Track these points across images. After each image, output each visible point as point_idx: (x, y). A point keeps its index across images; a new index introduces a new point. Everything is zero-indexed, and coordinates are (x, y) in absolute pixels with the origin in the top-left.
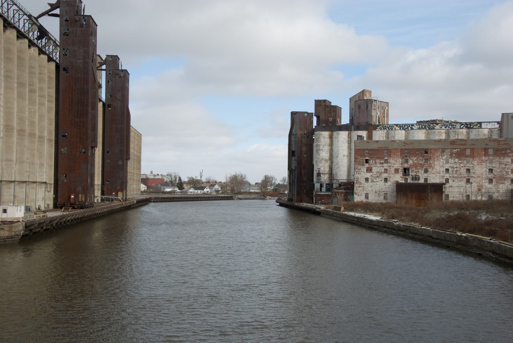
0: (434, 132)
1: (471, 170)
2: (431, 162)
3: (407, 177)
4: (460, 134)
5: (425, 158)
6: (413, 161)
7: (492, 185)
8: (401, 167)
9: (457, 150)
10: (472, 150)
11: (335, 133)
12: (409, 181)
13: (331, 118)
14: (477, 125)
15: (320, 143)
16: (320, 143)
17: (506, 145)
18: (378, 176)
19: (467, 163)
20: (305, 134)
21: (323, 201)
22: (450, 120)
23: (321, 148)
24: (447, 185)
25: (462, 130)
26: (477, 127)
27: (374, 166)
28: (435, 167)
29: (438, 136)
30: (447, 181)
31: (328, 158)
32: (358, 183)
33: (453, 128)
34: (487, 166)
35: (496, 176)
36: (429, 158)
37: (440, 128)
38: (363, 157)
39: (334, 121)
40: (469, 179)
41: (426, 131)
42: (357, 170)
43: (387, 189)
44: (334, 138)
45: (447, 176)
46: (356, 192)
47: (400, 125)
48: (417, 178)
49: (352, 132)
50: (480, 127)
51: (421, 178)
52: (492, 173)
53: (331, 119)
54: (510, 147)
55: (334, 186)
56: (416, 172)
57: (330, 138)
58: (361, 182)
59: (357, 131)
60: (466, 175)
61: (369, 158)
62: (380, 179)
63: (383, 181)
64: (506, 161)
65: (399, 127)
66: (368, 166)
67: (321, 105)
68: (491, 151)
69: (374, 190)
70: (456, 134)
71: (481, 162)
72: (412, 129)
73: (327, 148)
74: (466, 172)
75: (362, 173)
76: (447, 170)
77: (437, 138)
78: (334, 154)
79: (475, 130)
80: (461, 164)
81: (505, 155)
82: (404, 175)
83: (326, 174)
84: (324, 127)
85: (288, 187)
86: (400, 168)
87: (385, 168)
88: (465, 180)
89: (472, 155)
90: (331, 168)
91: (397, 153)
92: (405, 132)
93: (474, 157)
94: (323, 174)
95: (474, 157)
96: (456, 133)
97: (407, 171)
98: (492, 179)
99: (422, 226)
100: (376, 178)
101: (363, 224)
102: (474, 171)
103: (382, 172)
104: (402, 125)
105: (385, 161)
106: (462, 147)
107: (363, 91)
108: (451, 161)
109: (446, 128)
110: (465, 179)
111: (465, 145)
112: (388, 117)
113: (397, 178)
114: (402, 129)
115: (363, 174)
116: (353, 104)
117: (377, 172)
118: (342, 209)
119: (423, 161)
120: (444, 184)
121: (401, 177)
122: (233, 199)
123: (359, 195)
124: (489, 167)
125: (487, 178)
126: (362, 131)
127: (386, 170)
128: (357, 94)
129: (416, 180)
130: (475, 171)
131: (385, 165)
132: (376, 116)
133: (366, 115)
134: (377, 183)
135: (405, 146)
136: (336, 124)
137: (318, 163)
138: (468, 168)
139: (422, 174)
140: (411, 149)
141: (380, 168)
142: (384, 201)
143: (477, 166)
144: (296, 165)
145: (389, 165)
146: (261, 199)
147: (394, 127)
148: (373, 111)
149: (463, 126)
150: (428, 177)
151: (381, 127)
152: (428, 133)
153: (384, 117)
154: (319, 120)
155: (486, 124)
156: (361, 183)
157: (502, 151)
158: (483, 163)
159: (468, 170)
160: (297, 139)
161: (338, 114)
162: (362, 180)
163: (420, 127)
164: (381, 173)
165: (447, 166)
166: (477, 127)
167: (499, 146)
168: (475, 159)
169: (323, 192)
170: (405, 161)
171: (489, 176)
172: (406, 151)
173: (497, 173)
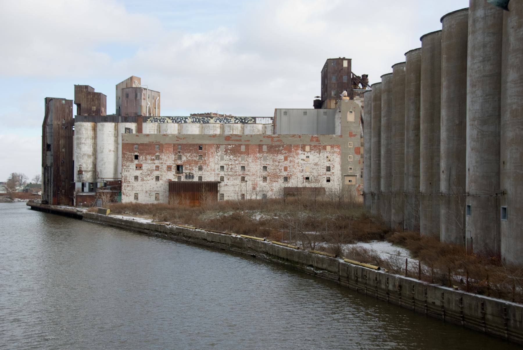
0: (209, 127)
2: (205, 159)
3: (181, 175)
4: (235, 129)
5: (199, 154)
6: (187, 158)
7: (267, 183)
8: (174, 164)
9: (232, 146)
10: (247, 146)
11: (99, 125)
12: (183, 179)
14: (251, 120)
17: (279, 141)
18: (148, 174)
19: (242, 160)
20: (63, 125)
21: (85, 203)
23: (83, 141)
26: (252, 122)
27: (144, 163)
28: (210, 164)
30: (222, 179)
32: (127, 182)
33: (228, 122)
37: (215, 122)
38: (132, 153)
40: (244, 177)
41: (200, 124)
42: (125, 167)
43: (159, 189)
44: (98, 130)
45: (222, 174)
46: (124, 192)
47: (173, 118)
50: (255, 122)
51: (195, 176)
52: (266, 170)
53: (94, 108)
54: (282, 144)
55: (99, 185)
56: (190, 169)
58: (129, 180)
59: (125, 123)
60: (241, 173)
61: (138, 154)
62: (151, 178)
63: (155, 179)
64: (279, 158)
66: (137, 163)
67: (82, 91)
68: (265, 148)
69: (144, 190)
70: (231, 129)
71: (255, 159)
72: (185, 122)
73: (90, 142)
75: (131, 171)
76: (222, 167)
78: (98, 148)
80: (236, 162)
81: (278, 152)
83: (89, 171)
84: (86, 117)
86: (173, 165)
87: (156, 165)
90: (95, 165)
91: (170, 149)
92: (179, 125)
93: (249, 154)
94: (85, 171)
96: (231, 128)
97: (180, 169)
98: (266, 177)
99: (196, 229)
100: (146, 176)
102: (249, 169)
103: (153, 170)
104: (175, 118)
105: (156, 157)
106: (237, 143)
107: (131, 78)
108: (226, 157)
109: (220, 122)
110: (240, 177)
112: (159, 108)
117: (148, 170)
118: (108, 211)
119: (198, 158)
120: (219, 182)
121: (173, 175)
123: (127, 196)
124: (263, 164)
125: (262, 176)
127: (157, 167)
128: (124, 81)
129: (189, 178)
131: (156, 162)
134: (148, 182)
135: (178, 140)
136: (100, 115)
137: (79, 159)
138: (243, 165)
139: (196, 172)
140: (184, 144)
141: (152, 165)
142: (156, 202)
145: (161, 161)
147: (165, 119)
148: (143, 100)
149: (238, 120)
151: (152, 119)
152: (202, 127)
153: (155, 108)
154: (80, 108)
155: (260, 119)
156: (129, 182)
158: (258, 161)
159: (243, 168)
161: (103, 103)
163: (193, 121)
164: (152, 171)
165: (222, 163)
166: (252, 122)
168: (249, 156)
170: (178, 157)
172: (179, 147)
173: (271, 171)
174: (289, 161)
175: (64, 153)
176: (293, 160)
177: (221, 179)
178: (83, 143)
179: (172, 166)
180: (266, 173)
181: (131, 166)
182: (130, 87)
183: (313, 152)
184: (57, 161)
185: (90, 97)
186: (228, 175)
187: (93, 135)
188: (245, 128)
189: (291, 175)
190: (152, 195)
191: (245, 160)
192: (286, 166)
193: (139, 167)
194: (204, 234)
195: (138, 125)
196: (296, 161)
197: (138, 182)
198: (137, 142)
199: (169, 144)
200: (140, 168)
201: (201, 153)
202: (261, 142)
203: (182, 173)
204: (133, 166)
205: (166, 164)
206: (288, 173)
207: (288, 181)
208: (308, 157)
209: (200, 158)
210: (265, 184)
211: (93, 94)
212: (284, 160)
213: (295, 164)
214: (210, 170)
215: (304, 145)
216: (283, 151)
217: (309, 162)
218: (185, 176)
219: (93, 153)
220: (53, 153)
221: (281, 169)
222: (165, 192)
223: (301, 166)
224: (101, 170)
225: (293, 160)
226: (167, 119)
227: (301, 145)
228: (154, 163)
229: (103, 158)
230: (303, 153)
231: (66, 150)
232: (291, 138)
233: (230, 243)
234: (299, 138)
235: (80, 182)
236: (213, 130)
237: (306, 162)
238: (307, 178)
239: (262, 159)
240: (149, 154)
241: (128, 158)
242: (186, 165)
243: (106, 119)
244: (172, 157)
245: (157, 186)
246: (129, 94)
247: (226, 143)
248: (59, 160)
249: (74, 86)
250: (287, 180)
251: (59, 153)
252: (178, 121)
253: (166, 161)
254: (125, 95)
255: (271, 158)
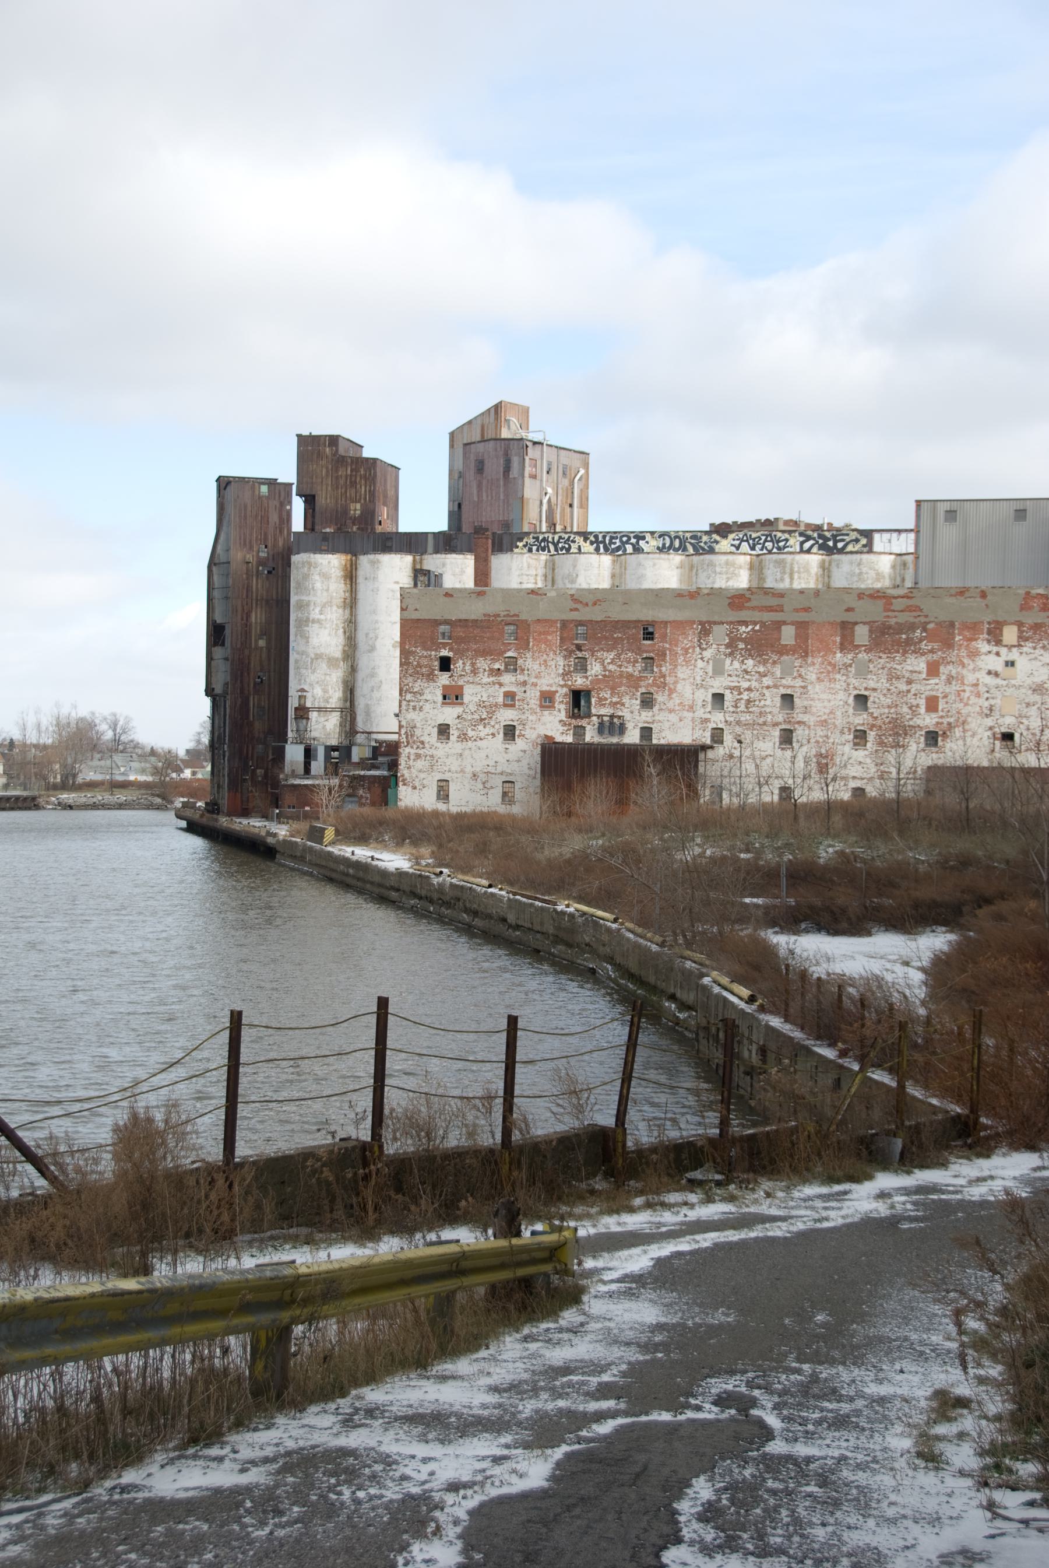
0: (711, 564)
1: (795, 700)
2: (664, 669)
3: (583, 722)
4: (799, 572)
5: (645, 655)
6: (604, 667)
7: (866, 752)
8: (562, 686)
9: (750, 627)
10: (801, 626)
11: (364, 560)
12: (591, 736)
13: (358, 506)
14: (857, 541)
15: (311, 598)
16: (311, 598)
17: (910, 611)
18: (482, 720)
19: (785, 674)
20: (261, 562)
21: (307, 808)
22: (826, 521)
23: (315, 614)
24: (720, 751)
25: (806, 556)
26: (858, 547)
27: (468, 682)
28: (679, 687)
29: (724, 576)
30: (718, 736)
31: (338, 654)
32: (414, 742)
33: (779, 548)
34: (848, 684)
35: (879, 722)
36: (657, 655)
37: (733, 549)
38: (431, 650)
39: (368, 517)
40: (791, 731)
41: (683, 557)
42: (409, 697)
43: (514, 767)
44: (360, 580)
45: (718, 719)
46: (407, 775)
47: (596, 537)
48: (614, 725)
49: (425, 557)
50: (869, 548)
51: (629, 726)
52: (866, 709)
53: (356, 509)
54: (923, 619)
55: (356, 755)
56: (614, 705)
57: (345, 577)
58: (422, 739)
59: (443, 556)
60: (780, 718)
61: (451, 654)
62: (489, 730)
63: (502, 735)
64: (910, 668)
65: (592, 543)
66: (447, 683)
67: (320, 455)
68: (862, 634)
69: (469, 769)
70: (784, 573)
71: (829, 672)
72: (637, 550)
73: (335, 616)
74: (782, 707)
75: (427, 707)
76: (719, 698)
77: (720, 583)
78: (361, 637)
79: (849, 556)
80: (764, 679)
81: (908, 647)
82: (573, 716)
83: (333, 710)
84: (325, 537)
85: (209, 756)
86: (559, 689)
87: (507, 689)
88: (776, 733)
89: (800, 647)
90: (350, 691)
91: (549, 638)
92: (614, 561)
93: (807, 655)
94: (320, 710)
95: (805, 654)
96: (784, 567)
97: (583, 703)
98: (865, 732)
99: (490, 886)
100: (474, 725)
101: (368, 886)
102: (806, 703)
103: (496, 705)
104: (604, 537)
105: (506, 665)
106: (768, 617)
107: (497, 408)
108: (733, 665)
109: (753, 548)
110: (778, 729)
111: (780, 609)
112: (584, 505)
113: (548, 726)
114: (602, 550)
115: (431, 711)
116: (459, 450)
117: (481, 705)
118: (330, 833)
119: (639, 666)
120: (704, 748)
121: (561, 721)
122: (37, 807)
123: (415, 788)
124: (855, 688)
125: (850, 730)
126: (461, 556)
127: (510, 696)
128: (476, 418)
129: (611, 733)
130: (811, 703)
131: (507, 678)
132: (538, 503)
133: (502, 497)
134: (479, 743)
135: (576, 609)
136: (373, 529)
137: (303, 671)
138: (789, 692)
139: (632, 712)
140: (597, 622)
141: (491, 690)
142: (502, 809)
143: (817, 686)
144: (229, 679)
145: (521, 678)
146: (150, 807)
147: (574, 542)
148: (527, 480)
149: (811, 542)
150: (653, 723)
151: (531, 541)
152: (692, 567)
153: (571, 506)
154: (314, 510)
155: (886, 536)
156: (422, 743)
157: (898, 634)
158: (838, 676)
159: (788, 700)
160: (231, 581)
161: (385, 491)
162: (426, 732)
163: (664, 545)
164: (492, 709)
165: (718, 685)
166: (858, 547)
167: (888, 617)
168: (810, 660)
169: (315, 777)
170: (576, 664)
171: (857, 721)
172: (581, 630)
173: (883, 711)
174: (943, 677)
175: (264, 655)
176: (958, 673)
177: (713, 736)
178: (313, 621)
179: (557, 692)
180: (865, 716)
181: (427, 691)
182: (494, 437)
183: (1028, 647)
184: (242, 675)
185: (345, 472)
186: (738, 723)
187: (347, 594)
188: (834, 569)
189: (949, 724)
190: (492, 788)
191: (795, 674)
192: (934, 693)
193: (452, 696)
194: (501, 901)
195: (477, 560)
196: (970, 678)
197: (450, 744)
198: (447, 617)
199: (546, 621)
200: (457, 698)
201: (649, 652)
202: (850, 613)
203: (589, 715)
204: (433, 692)
205: (538, 688)
206: (942, 717)
207: (940, 743)
208: (1011, 664)
209: (646, 666)
210: (860, 754)
211: (352, 462)
212: (928, 675)
213: (967, 688)
214: (677, 708)
215: (997, 622)
216: (923, 645)
217: (1013, 682)
218: (596, 726)
219: (344, 651)
220: (229, 650)
221: (918, 706)
222: (535, 778)
223: (987, 695)
224: (367, 706)
225: (958, 673)
226: (580, 540)
227: (989, 623)
228: (501, 685)
229: (374, 668)
230: (995, 649)
231: (269, 642)
232: (953, 600)
233: (551, 930)
234: (979, 599)
235: (301, 743)
236: (724, 576)
237: (1005, 683)
238: (1008, 737)
239: (853, 670)
240: (484, 653)
241: (419, 666)
242: (601, 690)
243: (389, 544)
244: (559, 662)
245: (507, 757)
246: (486, 462)
247: (730, 619)
248: (249, 674)
249: (294, 442)
250: (937, 741)
251: (247, 652)
252: (613, 546)
253: (536, 677)
254: (472, 465)
255: (883, 668)
